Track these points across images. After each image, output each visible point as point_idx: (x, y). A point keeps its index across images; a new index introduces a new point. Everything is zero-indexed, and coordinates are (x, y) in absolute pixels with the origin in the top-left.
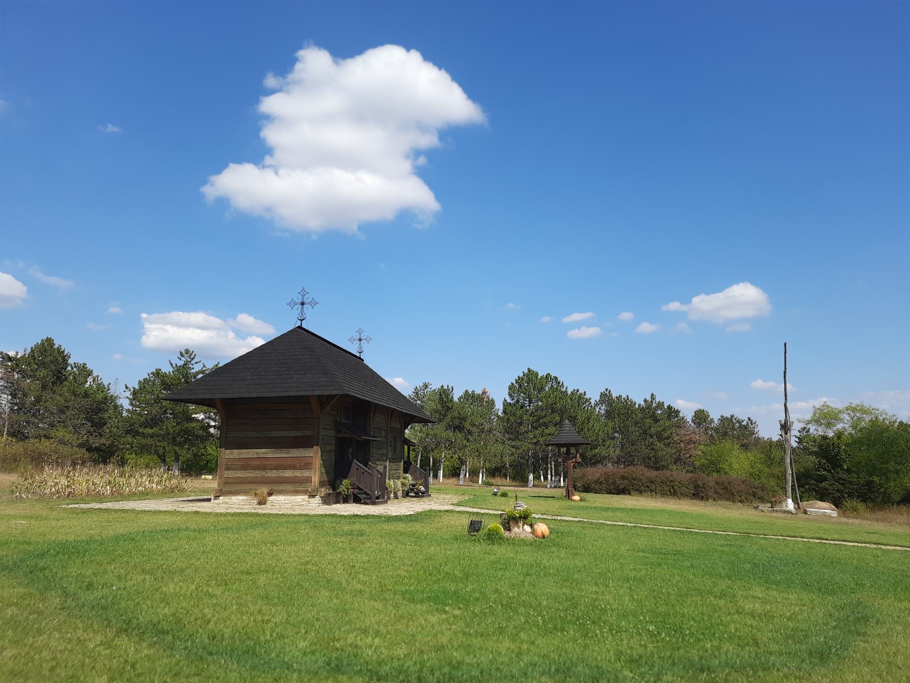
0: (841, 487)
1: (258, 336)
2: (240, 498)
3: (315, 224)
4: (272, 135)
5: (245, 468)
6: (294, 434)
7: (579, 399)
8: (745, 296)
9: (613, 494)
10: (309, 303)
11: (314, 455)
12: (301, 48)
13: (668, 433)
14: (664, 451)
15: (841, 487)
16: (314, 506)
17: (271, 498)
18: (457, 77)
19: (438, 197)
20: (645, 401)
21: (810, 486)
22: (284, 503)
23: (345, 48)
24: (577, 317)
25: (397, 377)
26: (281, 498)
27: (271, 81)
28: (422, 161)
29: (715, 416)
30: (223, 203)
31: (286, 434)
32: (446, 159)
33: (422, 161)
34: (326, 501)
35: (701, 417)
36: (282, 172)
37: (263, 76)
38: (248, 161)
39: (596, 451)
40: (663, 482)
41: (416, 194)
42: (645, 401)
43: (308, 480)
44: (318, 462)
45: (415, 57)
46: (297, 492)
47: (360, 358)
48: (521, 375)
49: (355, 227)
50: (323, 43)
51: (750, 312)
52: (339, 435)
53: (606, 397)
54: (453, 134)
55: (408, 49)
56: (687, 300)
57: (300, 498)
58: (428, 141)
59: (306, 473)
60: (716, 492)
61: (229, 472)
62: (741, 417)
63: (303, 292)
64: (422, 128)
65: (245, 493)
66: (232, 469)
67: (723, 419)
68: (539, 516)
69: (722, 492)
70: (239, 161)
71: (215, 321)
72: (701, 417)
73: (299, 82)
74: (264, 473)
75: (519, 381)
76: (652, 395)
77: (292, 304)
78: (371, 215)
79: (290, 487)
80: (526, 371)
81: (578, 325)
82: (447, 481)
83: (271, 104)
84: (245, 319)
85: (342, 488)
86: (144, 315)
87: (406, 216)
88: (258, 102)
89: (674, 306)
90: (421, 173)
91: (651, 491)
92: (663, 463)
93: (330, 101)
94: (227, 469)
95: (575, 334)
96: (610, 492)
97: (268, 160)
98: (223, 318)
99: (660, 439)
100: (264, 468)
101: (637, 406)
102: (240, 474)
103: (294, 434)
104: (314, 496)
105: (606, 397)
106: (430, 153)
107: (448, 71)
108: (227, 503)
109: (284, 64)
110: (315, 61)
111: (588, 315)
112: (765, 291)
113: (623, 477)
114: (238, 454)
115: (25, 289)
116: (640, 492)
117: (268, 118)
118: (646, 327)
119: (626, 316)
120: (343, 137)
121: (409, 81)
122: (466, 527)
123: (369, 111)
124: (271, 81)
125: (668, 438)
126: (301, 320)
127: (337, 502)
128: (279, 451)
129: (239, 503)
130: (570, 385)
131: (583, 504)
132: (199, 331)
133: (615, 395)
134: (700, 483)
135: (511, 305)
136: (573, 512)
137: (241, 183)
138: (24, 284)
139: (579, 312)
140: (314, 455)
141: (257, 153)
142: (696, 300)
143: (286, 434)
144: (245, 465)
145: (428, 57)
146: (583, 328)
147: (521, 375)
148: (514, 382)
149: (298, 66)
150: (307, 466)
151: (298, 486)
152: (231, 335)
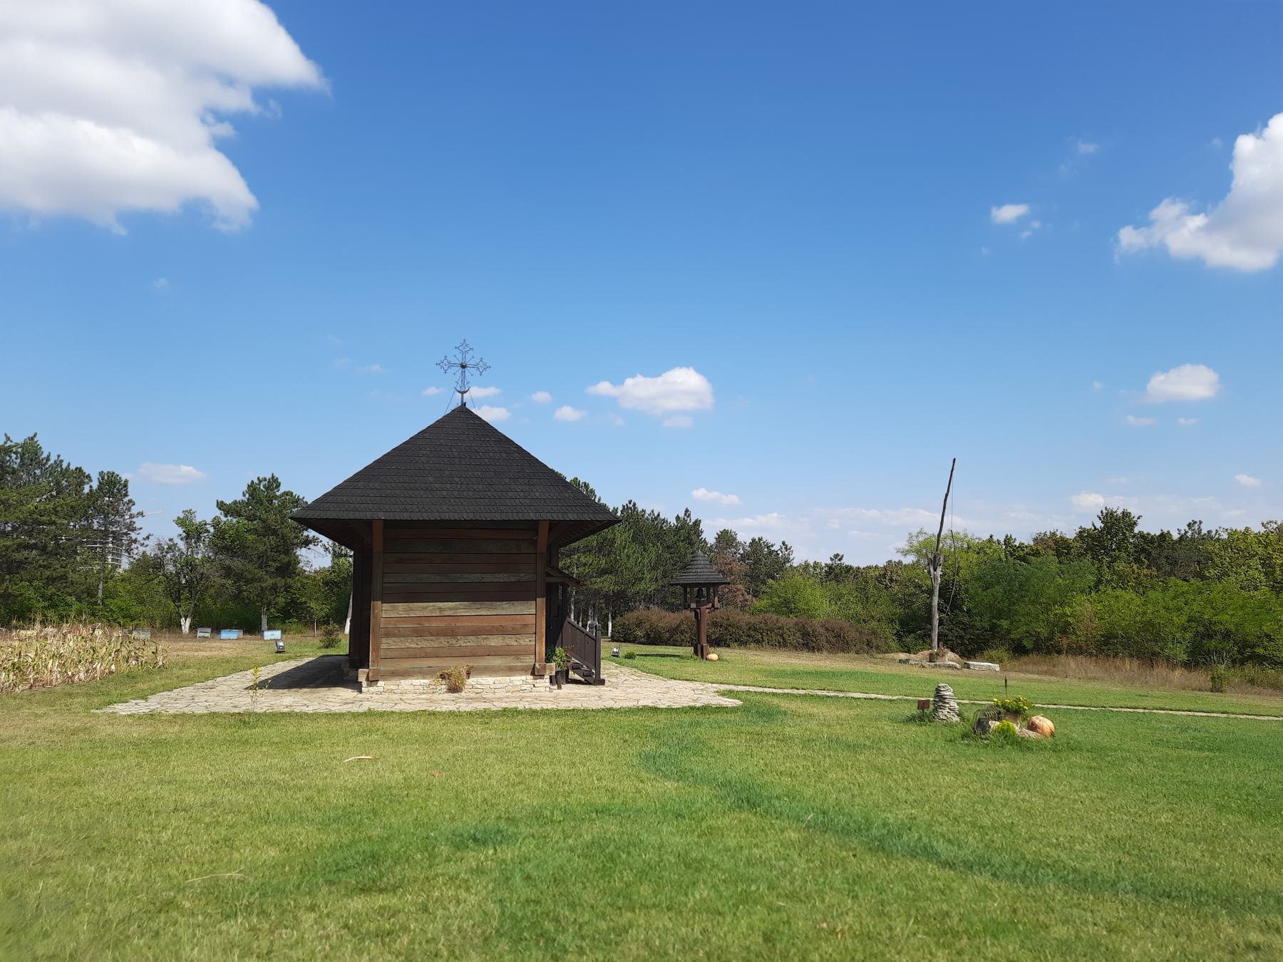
0: (962, 633)
5: (418, 633)
6: (503, 577)
8: (686, 382)
10: (476, 366)
15: (962, 633)
16: (542, 694)
17: (472, 681)
20: (678, 518)
21: (911, 630)
26: (487, 680)
29: (744, 537)
31: (488, 578)
33: (225, 130)
35: (726, 538)
41: (217, 179)
42: (678, 518)
51: (690, 404)
56: (618, 382)
58: (238, 100)
61: (390, 640)
62: (771, 541)
63: (464, 347)
64: (229, 81)
65: (421, 673)
66: (395, 636)
67: (755, 544)
69: (834, 640)
72: (726, 538)
74: (454, 642)
76: (687, 511)
77: (445, 365)
78: (141, 202)
79: (497, 662)
87: (196, 211)
89: (604, 387)
90: (221, 145)
91: (757, 642)
94: (387, 635)
102: (412, 644)
103: (503, 577)
106: (238, 120)
108: (392, 691)
112: (709, 381)
114: (406, 610)
116: (742, 643)
118: (567, 413)
119: (542, 397)
122: (927, 729)
126: (463, 393)
128: (478, 605)
136: (794, 682)
142: (629, 382)
143: (488, 578)
151: (510, 662)
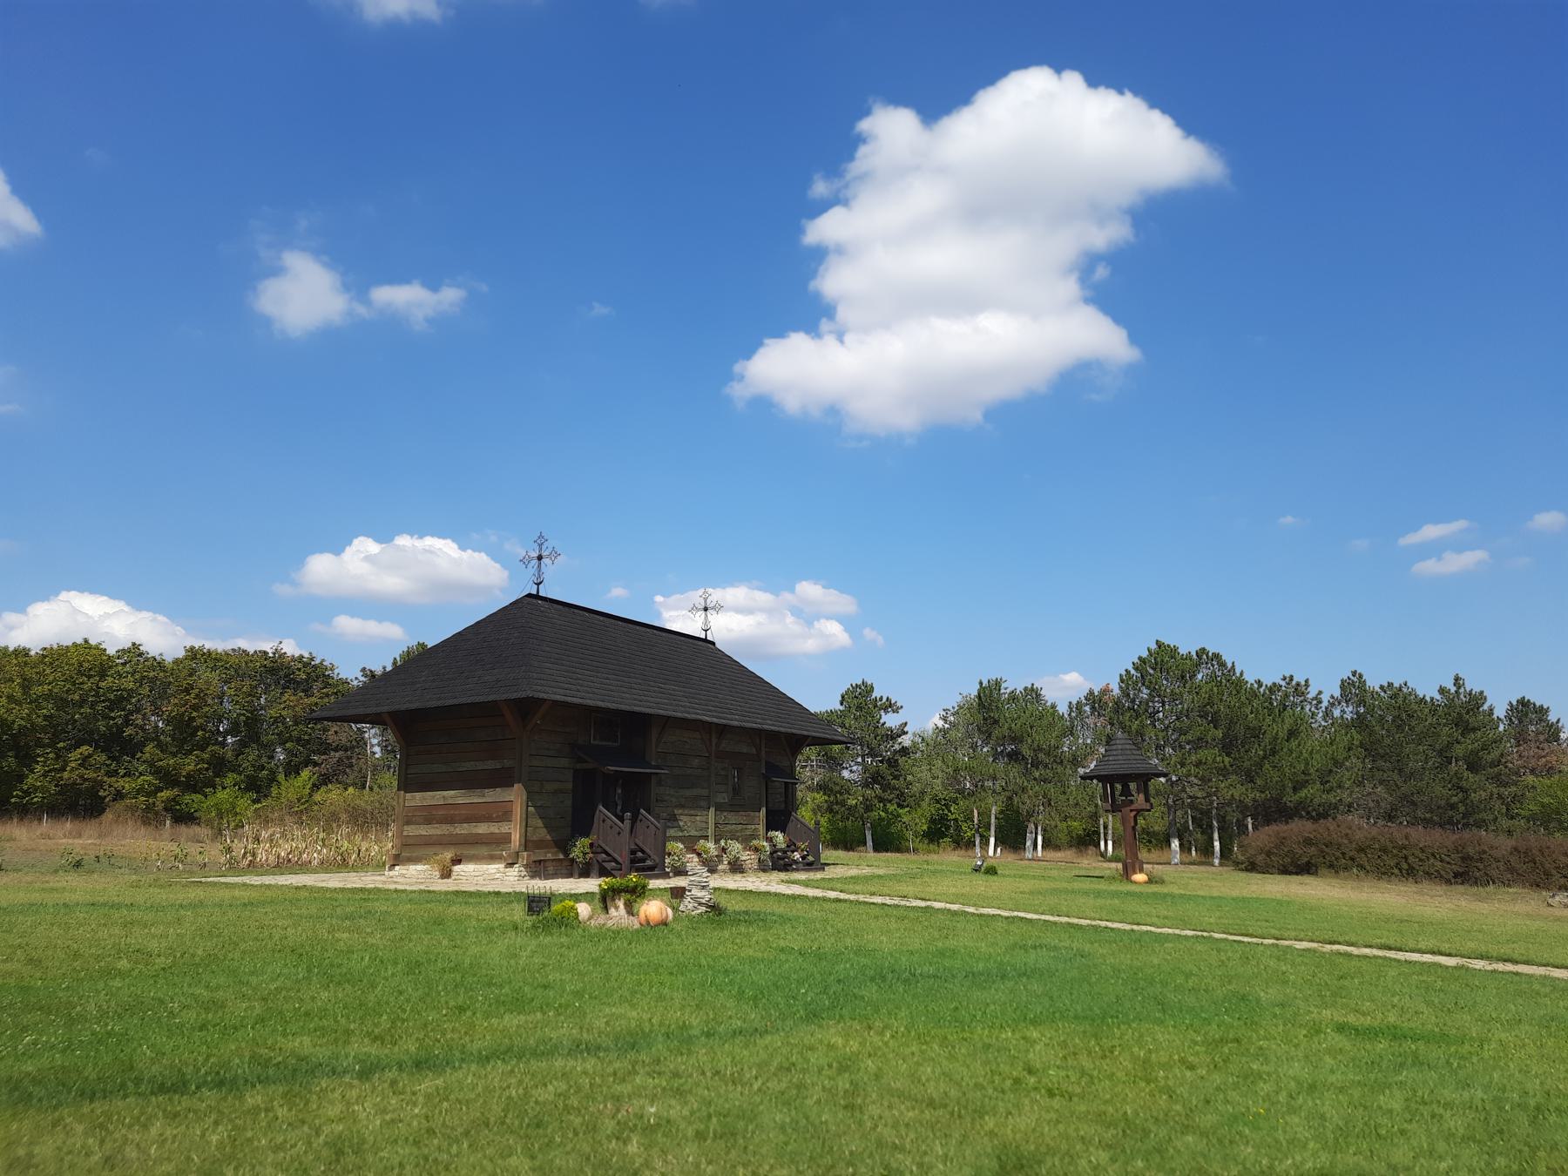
1: (828, 618)
2: (420, 867)
3: (907, 420)
4: (835, 282)
5: (428, 821)
6: (490, 765)
7: (1288, 697)
9: (1290, 873)
11: (515, 796)
12: (866, 112)
13: (1495, 754)
14: (1481, 788)
17: (456, 868)
18: (1157, 100)
19: (1134, 339)
20: (1442, 691)
22: (477, 875)
23: (939, 98)
24: (1431, 532)
25: (1066, 673)
27: (820, 188)
28: (1101, 272)
30: (764, 405)
32: (1146, 262)
33: (1101, 272)
34: (537, 869)
36: (848, 338)
37: (807, 183)
38: (796, 329)
39: (1303, 793)
40: (1384, 850)
41: (1094, 336)
42: (1442, 691)
43: (506, 839)
44: (518, 811)
45: (1073, 81)
46: (492, 859)
47: (705, 640)
48: (1145, 654)
49: (978, 416)
50: (897, 99)
52: (578, 766)
53: (1353, 688)
54: (1160, 217)
55: (1058, 68)
57: (495, 868)
58: (1101, 237)
59: (504, 828)
60: (1512, 870)
68: (937, 905)
70: (780, 333)
71: (763, 598)
73: (862, 177)
75: (1141, 665)
76: (1457, 679)
79: (484, 851)
80: (1154, 646)
81: (1434, 549)
82: (1051, 855)
83: (828, 228)
84: (809, 590)
85: (576, 853)
86: (659, 599)
87: (1075, 381)
88: (801, 231)
92: (1483, 815)
93: (923, 197)
95: (1429, 567)
96: (1285, 871)
97: (825, 325)
98: (773, 589)
99: (1473, 767)
100: (450, 820)
101: (1486, 707)
103: (490, 765)
104: (511, 865)
105: (1353, 688)
106: (1116, 258)
107: (1136, 93)
109: (835, 148)
110: (892, 129)
111: (1459, 525)
113: (1308, 842)
115: (506, 574)
117: (819, 255)
120: (947, 258)
121: (1083, 125)
123: (988, 204)
124: (820, 188)
125: (1494, 764)
127: (570, 875)
129: (415, 876)
130: (1259, 667)
131: (1154, 888)
132: (740, 617)
133: (1374, 682)
134: (1471, 851)
135: (1289, 519)
137: (787, 367)
138: (504, 567)
139: (1437, 522)
140: (515, 796)
141: (811, 314)
143: (481, 766)
144: (429, 816)
145: (1094, 80)
146: (1448, 555)
147: (1145, 654)
148: (1130, 668)
149: (863, 150)
150: (505, 816)
151: (490, 848)
152: (790, 619)
